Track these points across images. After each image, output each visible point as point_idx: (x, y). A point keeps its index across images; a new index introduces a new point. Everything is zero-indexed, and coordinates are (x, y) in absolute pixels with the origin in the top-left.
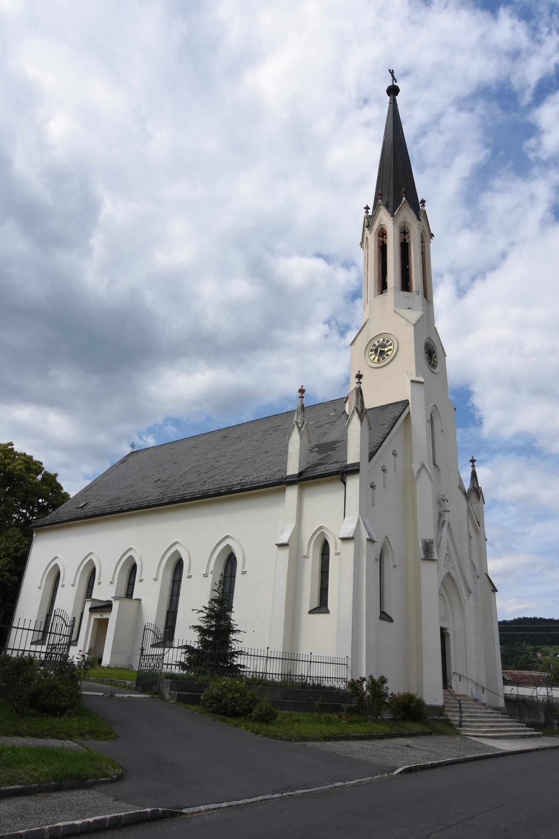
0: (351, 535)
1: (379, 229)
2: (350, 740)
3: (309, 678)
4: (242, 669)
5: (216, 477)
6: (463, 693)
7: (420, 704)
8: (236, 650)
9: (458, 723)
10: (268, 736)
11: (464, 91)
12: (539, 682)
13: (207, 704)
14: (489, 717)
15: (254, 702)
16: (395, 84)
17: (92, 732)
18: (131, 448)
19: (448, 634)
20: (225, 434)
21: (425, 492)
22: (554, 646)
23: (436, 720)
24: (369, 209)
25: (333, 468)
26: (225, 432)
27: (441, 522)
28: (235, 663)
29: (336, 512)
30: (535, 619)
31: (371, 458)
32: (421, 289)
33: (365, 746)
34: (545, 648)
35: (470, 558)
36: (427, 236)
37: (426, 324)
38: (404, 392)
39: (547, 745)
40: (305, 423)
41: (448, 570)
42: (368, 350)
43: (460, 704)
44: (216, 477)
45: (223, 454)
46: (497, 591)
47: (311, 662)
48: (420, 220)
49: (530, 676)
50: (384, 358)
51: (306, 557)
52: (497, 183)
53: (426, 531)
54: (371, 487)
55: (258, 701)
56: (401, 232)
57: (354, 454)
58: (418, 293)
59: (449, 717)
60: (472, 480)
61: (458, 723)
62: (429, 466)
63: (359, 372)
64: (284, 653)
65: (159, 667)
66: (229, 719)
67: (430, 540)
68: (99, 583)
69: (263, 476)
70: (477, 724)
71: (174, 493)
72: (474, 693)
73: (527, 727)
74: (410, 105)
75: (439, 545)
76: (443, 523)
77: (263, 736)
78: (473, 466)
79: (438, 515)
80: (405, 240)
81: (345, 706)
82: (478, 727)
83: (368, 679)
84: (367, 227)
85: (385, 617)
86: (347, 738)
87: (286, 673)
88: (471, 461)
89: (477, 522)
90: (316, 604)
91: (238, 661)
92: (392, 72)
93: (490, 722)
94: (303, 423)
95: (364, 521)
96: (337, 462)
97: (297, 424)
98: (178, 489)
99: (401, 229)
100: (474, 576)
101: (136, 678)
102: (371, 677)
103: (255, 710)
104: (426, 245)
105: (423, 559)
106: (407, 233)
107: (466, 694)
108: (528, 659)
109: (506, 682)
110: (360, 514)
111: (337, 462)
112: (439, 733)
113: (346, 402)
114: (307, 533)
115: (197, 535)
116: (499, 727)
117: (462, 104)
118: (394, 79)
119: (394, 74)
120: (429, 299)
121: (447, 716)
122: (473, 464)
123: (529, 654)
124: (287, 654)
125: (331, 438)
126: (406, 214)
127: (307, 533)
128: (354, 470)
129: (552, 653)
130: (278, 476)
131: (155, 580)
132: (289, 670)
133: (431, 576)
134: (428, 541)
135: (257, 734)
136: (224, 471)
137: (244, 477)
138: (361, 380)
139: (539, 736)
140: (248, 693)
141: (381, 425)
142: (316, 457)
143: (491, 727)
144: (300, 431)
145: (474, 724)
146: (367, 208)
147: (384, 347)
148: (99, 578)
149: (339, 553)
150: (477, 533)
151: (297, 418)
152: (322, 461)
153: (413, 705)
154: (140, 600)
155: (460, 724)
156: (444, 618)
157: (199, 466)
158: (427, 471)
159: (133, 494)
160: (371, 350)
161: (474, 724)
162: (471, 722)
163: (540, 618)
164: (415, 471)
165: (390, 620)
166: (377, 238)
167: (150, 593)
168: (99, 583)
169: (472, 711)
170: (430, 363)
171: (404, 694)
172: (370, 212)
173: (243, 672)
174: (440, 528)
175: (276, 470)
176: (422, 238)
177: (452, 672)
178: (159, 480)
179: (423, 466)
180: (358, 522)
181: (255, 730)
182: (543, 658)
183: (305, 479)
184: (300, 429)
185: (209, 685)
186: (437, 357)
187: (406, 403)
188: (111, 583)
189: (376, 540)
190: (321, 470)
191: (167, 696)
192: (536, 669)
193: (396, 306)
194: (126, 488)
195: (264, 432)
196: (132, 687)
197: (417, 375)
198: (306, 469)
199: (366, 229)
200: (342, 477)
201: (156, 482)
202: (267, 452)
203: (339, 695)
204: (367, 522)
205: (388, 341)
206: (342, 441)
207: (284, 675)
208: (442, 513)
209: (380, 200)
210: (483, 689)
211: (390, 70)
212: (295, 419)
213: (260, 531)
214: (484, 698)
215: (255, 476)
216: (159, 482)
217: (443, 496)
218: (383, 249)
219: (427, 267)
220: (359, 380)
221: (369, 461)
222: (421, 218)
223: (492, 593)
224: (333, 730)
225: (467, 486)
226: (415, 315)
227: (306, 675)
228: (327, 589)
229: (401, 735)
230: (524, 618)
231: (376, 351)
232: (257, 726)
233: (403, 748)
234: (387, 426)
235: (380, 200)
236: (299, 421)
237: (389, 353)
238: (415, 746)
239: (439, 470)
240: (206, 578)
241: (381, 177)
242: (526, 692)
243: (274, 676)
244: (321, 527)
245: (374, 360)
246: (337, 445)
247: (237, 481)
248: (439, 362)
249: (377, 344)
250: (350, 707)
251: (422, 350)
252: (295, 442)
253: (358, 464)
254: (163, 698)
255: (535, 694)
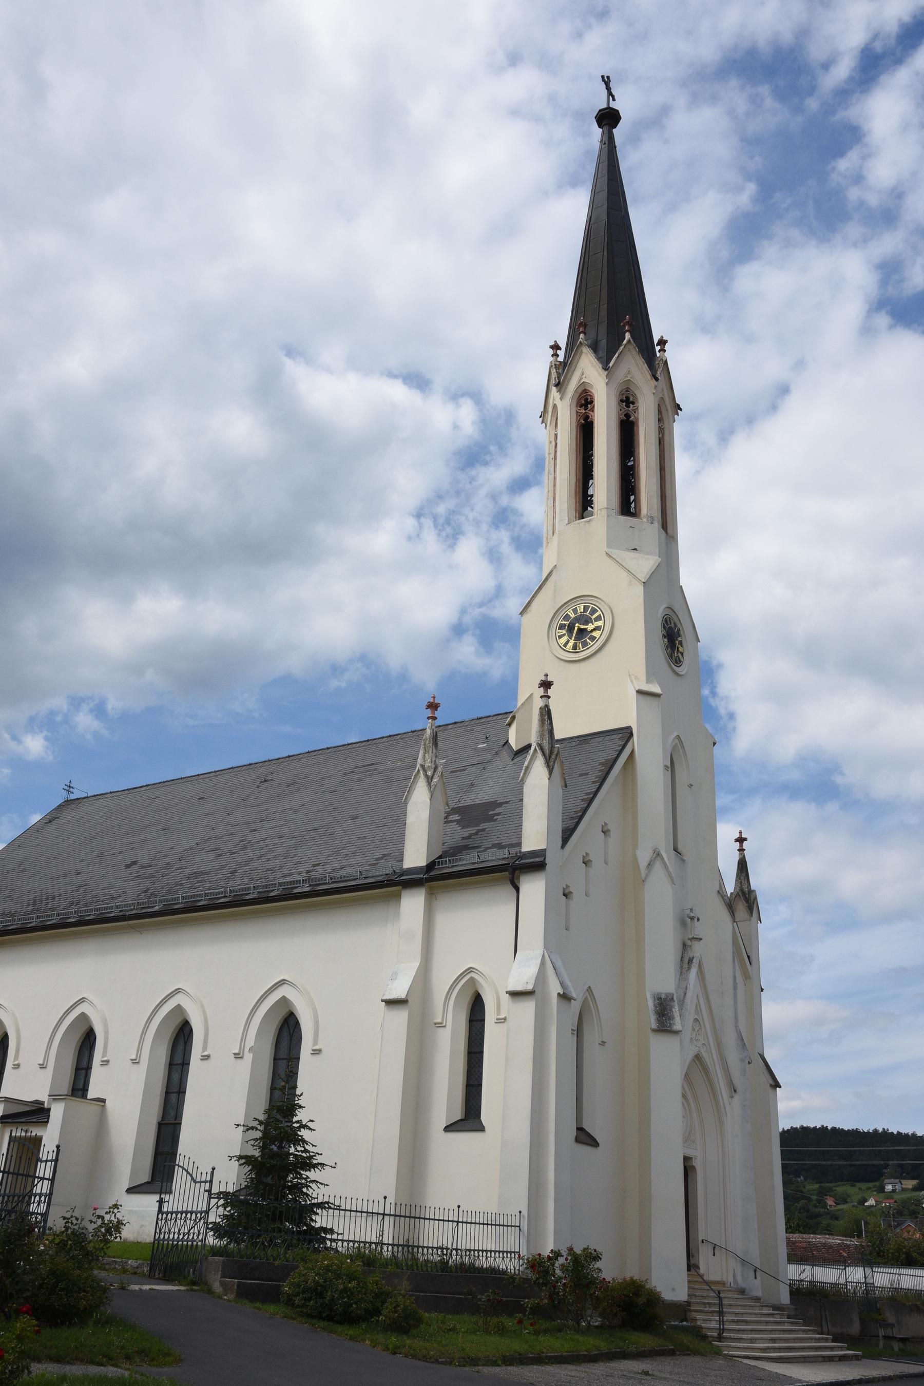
0: (530, 987)
1: (580, 391)
2: (546, 1363)
3: (454, 1252)
4: (329, 1236)
5: (256, 864)
6: (718, 1279)
7: (654, 1299)
8: (320, 1200)
9: (715, 1334)
10: (414, 1357)
11: (707, 51)
12: (841, 1255)
13: (297, 1301)
14: (767, 1323)
15: (382, 1296)
16: (613, 105)
17: (143, 1353)
18: (65, 793)
19: (694, 1168)
20: (263, 773)
21: (660, 900)
22: (859, 1185)
23: (675, 1327)
24: (560, 349)
25: (493, 857)
26: (262, 770)
27: (686, 960)
28: (318, 1225)
29: (496, 942)
30: (824, 1129)
31: (565, 841)
32: (657, 514)
33: (573, 1374)
34: (842, 1188)
35: (736, 1026)
36: (668, 407)
37: (664, 581)
38: (622, 711)
39: (889, 1373)
40: (440, 769)
41: (695, 1050)
42: (555, 625)
43: (720, 1299)
44: (256, 864)
45: (263, 816)
46: (780, 1087)
47: (458, 1222)
48: (657, 379)
49: (824, 1245)
50: (585, 644)
51: (440, 1025)
52: (770, 250)
53: (661, 976)
54: (564, 895)
55: (388, 1295)
56: (622, 401)
57: (535, 833)
58: (651, 520)
59: (699, 1323)
60: (738, 876)
61: (715, 1334)
62: (667, 854)
63: (546, 675)
64: (398, 1205)
65: (198, 1235)
66: (340, 1328)
67: (667, 995)
68: (17, 1066)
69: (354, 866)
70: (750, 1336)
71: (169, 892)
72: (739, 1279)
73: (833, 1341)
74: (634, 139)
75: (682, 1003)
76: (690, 961)
77: (406, 1356)
78: (741, 850)
79: (680, 946)
80: (628, 416)
81: (529, 1303)
82: (752, 1341)
83: (564, 1253)
84: (557, 385)
85: (584, 1137)
86: (539, 1360)
87: (401, 1243)
88: (737, 840)
89: (745, 956)
90: (458, 1115)
91: (321, 1220)
92: (606, 81)
93: (771, 1331)
94: (436, 769)
95: (554, 960)
96: (500, 846)
97: (425, 771)
98: (177, 885)
99: (621, 394)
100: (742, 1060)
101: (149, 1257)
102: (571, 1250)
103: (385, 1312)
104: (666, 426)
105: (654, 1031)
106: (633, 403)
107: (724, 1279)
108: (808, 1210)
109: (797, 1256)
110: (546, 947)
111: (500, 846)
112: (686, 1351)
113: (510, 724)
114: (444, 978)
115: (219, 978)
116: (787, 1340)
117: (704, 81)
118: (610, 94)
119: (611, 85)
120: (670, 531)
121: (695, 1320)
122: (741, 845)
123: (809, 1199)
124: (403, 1206)
125: (484, 794)
126: (631, 365)
127: (444, 978)
128: (535, 864)
129: (856, 1198)
130: (384, 869)
131: (135, 1062)
132: (406, 1237)
133: (668, 1060)
134: (663, 996)
135: (394, 1353)
136: (270, 851)
137: (314, 866)
138: (550, 692)
139: (857, 1358)
140: (370, 1279)
141: (581, 775)
142: (457, 833)
143: (774, 1340)
144: (429, 784)
145: (745, 1336)
146: (556, 347)
147: (587, 623)
148: (16, 1057)
149: (505, 1019)
150: (747, 976)
151: (423, 757)
152: (470, 842)
153: (642, 1300)
154: (104, 1101)
155: (720, 1334)
156: (688, 1139)
157: (217, 837)
158: (665, 864)
159: (82, 889)
160: (562, 627)
161: (745, 1336)
162: (739, 1331)
163: (834, 1129)
164: (643, 862)
165: (594, 1143)
166: (574, 409)
167: (124, 1086)
168: (17, 1066)
169: (737, 1311)
170: (671, 656)
171: (632, 1279)
172: (561, 354)
173: (332, 1240)
174: (684, 971)
175: (378, 854)
176: (660, 412)
177: (700, 1239)
178: (134, 863)
179: (657, 854)
180: (543, 963)
181: (391, 1346)
182: (839, 1207)
183: (437, 877)
184: (429, 780)
185: (298, 1267)
186: (684, 643)
187: (626, 734)
188: (42, 1066)
189: (574, 995)
190: (468, 861)
191: (217, 1287)
192: (829, 1231)
193: (609, 545)
194: (65, 875)
195: (345, 774)
196: (139, 1271)
197: (648, 681)
198: (440, 857)
199: (554, 390)
200: (513, 877)
201: (128, 866)
202: (355, 818)
203: (514, 1282)
204: (559, 964)
205: (594, 611)
206: (507, 802)
207: (398, 1246)
208: (689, 943)
209: (582, 336)
210: (755, 1271)
211: (603, 77)
212: (420, 761)
213: (355, 977)
214: (756, 1287)
215: (337, 866)
216: (135, 867)
217: (691, 910)
218: (585, 432)
219: (667, 469)
220: (546, 691)
221: (563, 846)
222: (658, 374)
223: (770, 1090)
224: (516, 1346)
225: (730, 887)
226: (645, 564)
227: (450, 1246)
228: (480, 1085)
229: (624, 1355)
230: (802, 1127)
231: (570, 629)
232: (393, 1339)
233: (638, 1376)
234: (592, 777)
235: (582, 336)
236: (428, 764)
237: (596, 634)
238: (658, 1374)
239: (683, 861)
240: (239, 1061)
241: (583, 289)
242: (826, 1275)
243: (425, 1250)
244: (470, 970)
245: (565, 645)
246: (498, 810)
247: (299, 873)
248: (686, 654)
249: (573, 616)
250: (538, 1304)
251: (658, 631)
252: (420, 808)
253: (542, 853)
254: (210, 1292)
255: (842, 1281)
